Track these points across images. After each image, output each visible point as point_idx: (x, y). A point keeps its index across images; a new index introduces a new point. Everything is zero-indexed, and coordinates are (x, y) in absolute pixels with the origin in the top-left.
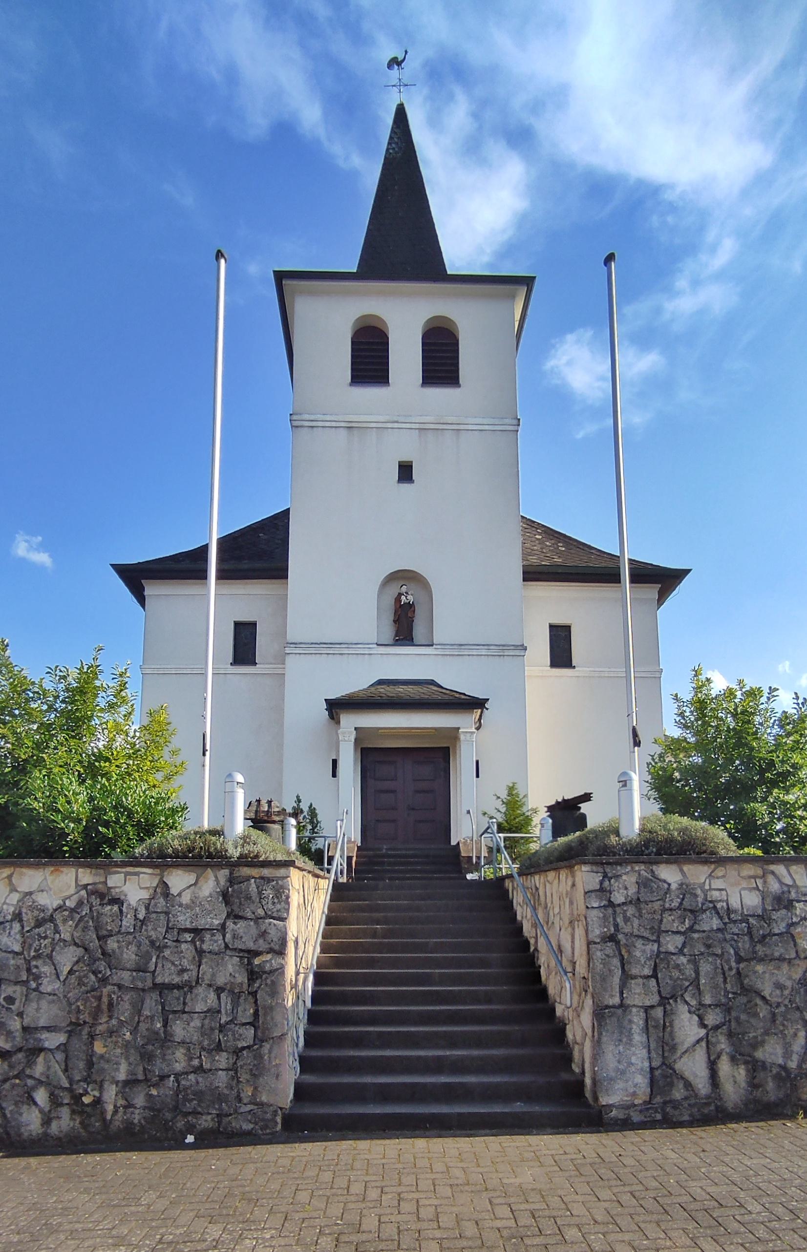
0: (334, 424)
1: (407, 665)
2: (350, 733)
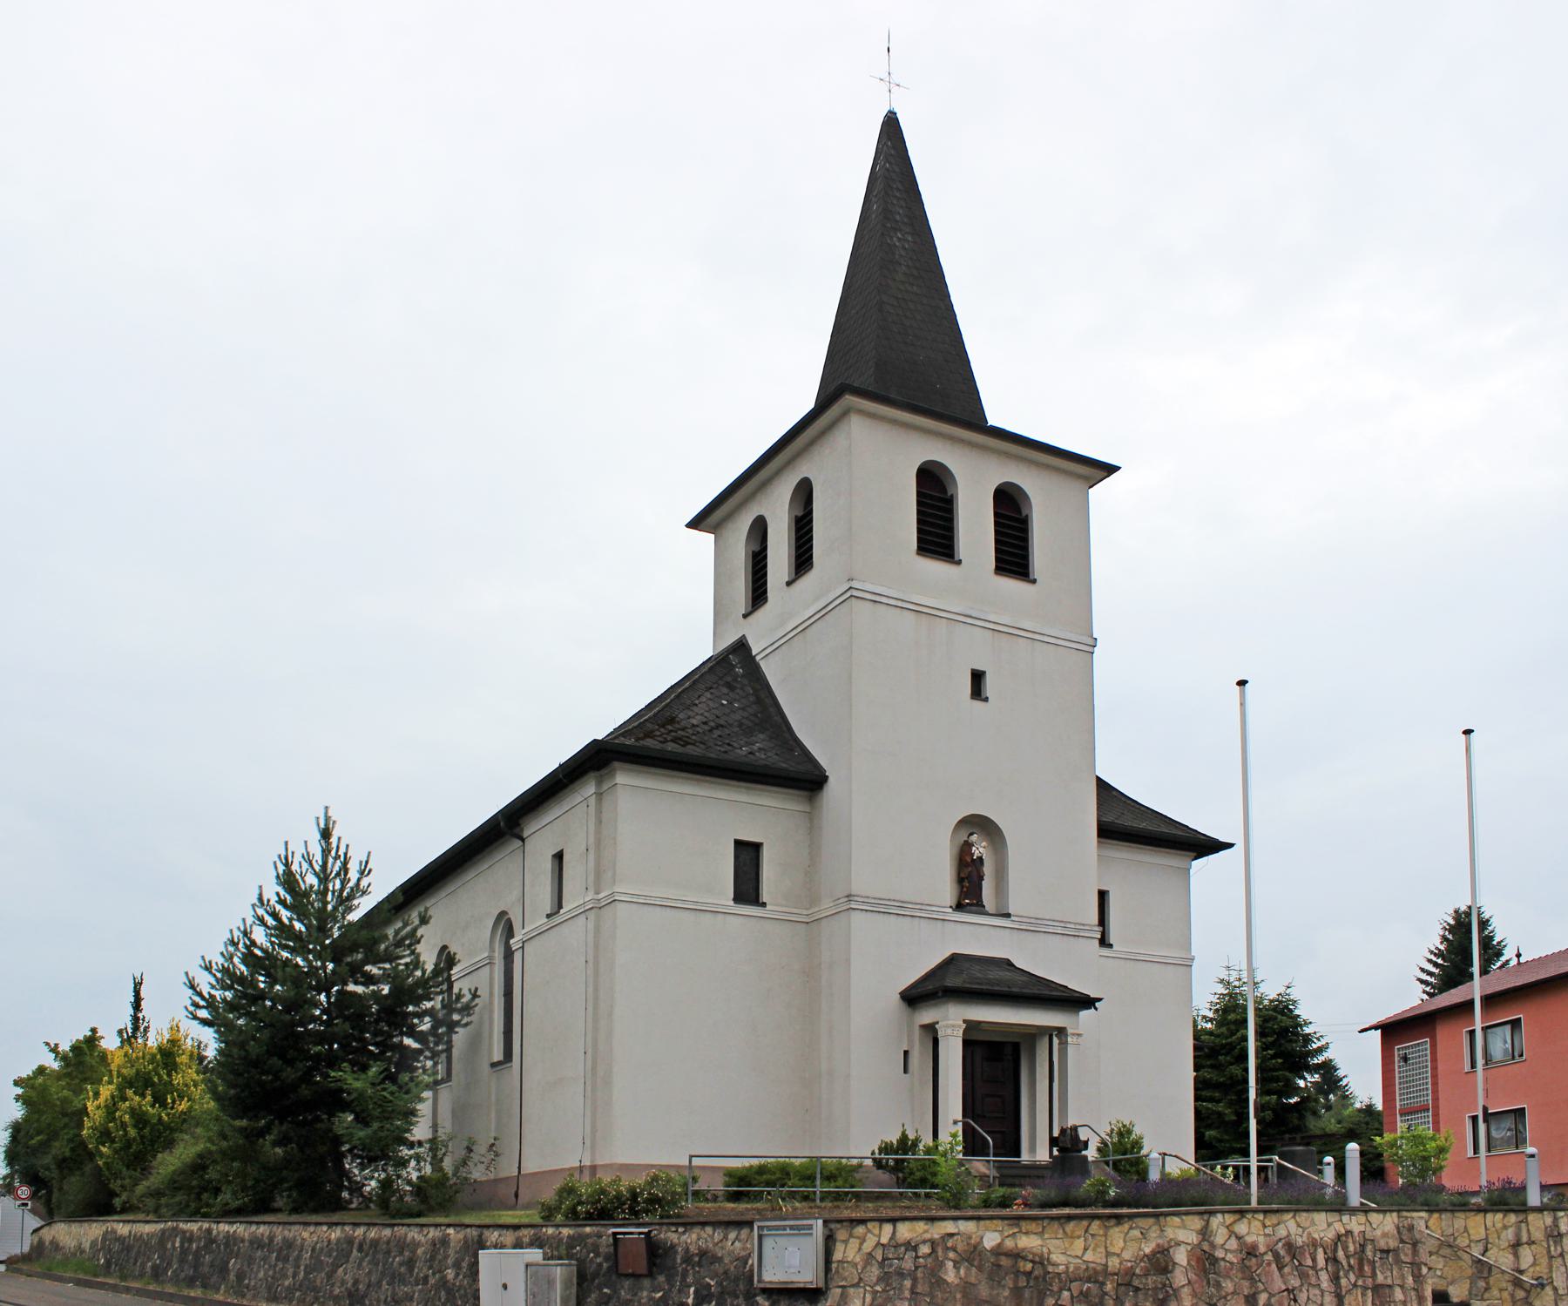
0: (899, 604)
1: (977, 938)
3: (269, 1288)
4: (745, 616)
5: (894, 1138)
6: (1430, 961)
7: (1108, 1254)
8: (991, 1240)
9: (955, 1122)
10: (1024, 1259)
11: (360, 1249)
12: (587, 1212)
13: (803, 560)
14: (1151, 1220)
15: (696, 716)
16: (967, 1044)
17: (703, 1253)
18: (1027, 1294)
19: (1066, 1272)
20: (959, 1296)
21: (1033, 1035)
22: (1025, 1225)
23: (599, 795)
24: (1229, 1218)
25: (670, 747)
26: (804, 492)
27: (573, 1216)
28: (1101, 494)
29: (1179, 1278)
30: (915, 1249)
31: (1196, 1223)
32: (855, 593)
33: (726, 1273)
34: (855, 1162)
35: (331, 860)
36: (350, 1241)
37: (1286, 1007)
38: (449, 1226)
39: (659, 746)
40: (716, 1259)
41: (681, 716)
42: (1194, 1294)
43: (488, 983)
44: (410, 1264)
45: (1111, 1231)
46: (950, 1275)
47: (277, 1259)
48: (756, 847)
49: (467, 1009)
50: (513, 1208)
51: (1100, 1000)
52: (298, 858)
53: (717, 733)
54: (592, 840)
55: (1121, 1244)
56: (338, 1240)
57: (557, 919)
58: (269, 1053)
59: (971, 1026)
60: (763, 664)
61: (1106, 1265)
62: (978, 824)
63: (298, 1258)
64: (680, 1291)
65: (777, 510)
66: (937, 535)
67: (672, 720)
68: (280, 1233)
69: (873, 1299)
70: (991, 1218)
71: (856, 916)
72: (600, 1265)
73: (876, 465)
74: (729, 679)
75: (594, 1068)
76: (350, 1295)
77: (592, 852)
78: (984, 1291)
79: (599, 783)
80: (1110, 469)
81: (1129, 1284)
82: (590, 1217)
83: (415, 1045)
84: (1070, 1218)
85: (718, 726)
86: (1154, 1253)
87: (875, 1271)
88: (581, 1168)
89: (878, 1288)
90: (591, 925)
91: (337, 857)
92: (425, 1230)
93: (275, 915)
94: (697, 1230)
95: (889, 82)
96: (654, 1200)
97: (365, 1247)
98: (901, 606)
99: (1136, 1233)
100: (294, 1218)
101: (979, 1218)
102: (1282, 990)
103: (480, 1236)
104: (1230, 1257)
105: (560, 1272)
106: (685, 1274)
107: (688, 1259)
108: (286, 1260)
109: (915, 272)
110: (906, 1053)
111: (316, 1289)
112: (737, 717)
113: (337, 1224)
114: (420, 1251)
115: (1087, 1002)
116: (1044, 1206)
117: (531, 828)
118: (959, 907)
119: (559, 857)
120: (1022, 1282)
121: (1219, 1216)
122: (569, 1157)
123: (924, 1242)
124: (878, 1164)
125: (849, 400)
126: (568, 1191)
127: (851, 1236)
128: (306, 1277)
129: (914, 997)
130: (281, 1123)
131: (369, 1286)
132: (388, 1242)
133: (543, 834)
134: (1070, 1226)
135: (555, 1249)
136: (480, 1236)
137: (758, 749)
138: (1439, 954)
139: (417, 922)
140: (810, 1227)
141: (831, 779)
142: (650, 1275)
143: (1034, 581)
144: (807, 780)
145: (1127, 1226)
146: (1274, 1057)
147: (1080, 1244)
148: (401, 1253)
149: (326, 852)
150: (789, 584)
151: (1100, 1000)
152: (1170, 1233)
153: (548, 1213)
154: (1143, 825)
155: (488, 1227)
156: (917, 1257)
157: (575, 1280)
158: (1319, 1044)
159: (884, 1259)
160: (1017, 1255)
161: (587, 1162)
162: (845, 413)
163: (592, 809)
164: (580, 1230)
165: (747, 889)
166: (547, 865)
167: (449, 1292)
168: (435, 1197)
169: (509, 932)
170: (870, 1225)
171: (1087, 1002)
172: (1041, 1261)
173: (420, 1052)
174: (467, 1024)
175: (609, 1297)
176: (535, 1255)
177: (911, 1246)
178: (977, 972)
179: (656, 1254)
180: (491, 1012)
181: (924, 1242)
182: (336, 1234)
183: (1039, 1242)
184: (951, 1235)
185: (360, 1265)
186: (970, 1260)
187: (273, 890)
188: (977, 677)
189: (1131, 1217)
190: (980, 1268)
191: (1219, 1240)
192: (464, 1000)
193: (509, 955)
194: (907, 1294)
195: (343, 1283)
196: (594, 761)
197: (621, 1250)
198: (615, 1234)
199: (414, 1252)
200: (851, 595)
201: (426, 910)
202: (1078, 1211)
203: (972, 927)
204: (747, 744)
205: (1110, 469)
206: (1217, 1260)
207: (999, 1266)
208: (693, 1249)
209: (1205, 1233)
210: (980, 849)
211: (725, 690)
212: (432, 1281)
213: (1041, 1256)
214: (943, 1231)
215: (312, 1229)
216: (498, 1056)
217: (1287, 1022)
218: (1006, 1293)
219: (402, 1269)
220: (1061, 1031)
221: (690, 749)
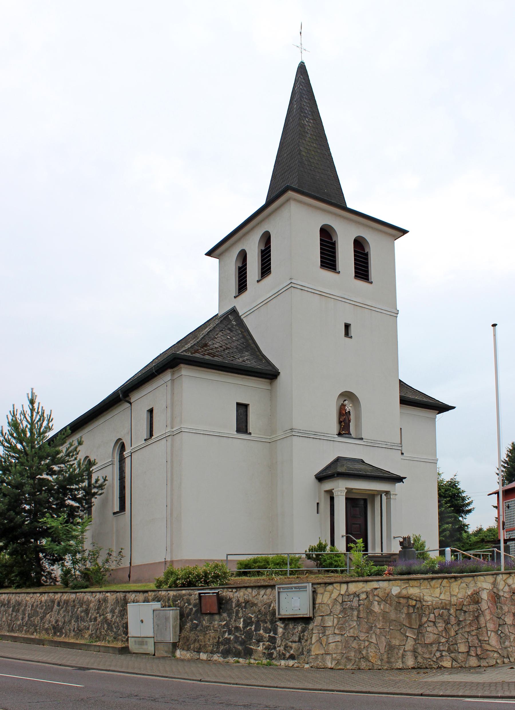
0: (313, 291)
1: (348, 449)
2: (344, 491)
3: (9, 626)
4: (235, 297)
5: (315, 544)
6: (502, 465)
7: (451, 595)
8: (395, 590)
9: (343, 536)
10: (412, 599)
11: (59, 605)
12: (183, 583)
13: (265, 269)
14: (471, 579)
15: (217, 343)
16: (348, 500)
17: (247, 602)
18: (413, 616)
19: (432, 605)
20: (381, 618)
21: (380, 493)
22: (411, 583)
23: (173, 380)
24: (505, 576)
25: (207, 357)
26: (267, 239)
27: (174, 586)
28: (400, 243)
29: (484, 606)
30: (358, 596)
31: (491, 579)
32: (293, 285)
33: (259, 611)
34: (297, 556)
35: (35, 414)
36: (53, 601)
37: (454, 485)
38: (107, 592)
39: (202, 357)
40: (254, 605)
41: (210, 343)
42: (491, 613)
43: (112, 475)
44: (87, 612)
45: (452, 585)
46: (376, 608)
47: (13, 611)
48: (246, 406)
49: (101, 487)
50: (129, 582)
51: (405, 478)
52: (19, 412)
53: (227, 351)
54: (169, 401)
55: (457, 590)
56: (46, 601)
57: (150, 441)
58: (8, 510)
59: (349, 491)
60: (244, 320)
61: (450, 601)
62: (348, 396)
63: (25, 610)
64: (235, 621)
65: (253, 248)
66: (329, 260)
67: (206, 345)
68: (14, 598)
69: (338, 622)
70: (395, 580)
71: (294, 438)
72: (191, 609)
73: (299, 226)
74: (229, 326)
75: (171, 514)
76: (54, 628)
77: (169, 409)
78: (393, 616)
79: (173, 374)
80: (404, 232)
81: (461, 610)
82: (183, 585)
83: (77, 505)
84: (433, 579)
85: (227, 348)
86: (472, 594)
87: (338, 608)
88: (165, 562)
89: (340, 616)
90: (169, 443)
91: (38, 413)
92: (94, 594)
93: (8, 441)
94: (243, 590)
95: (301, 48)
96: (217, 577)
97: (61, 604)
98: (313, 292)
99: (464, 585)
100: (18, 590)
101: (389, 580)
102: (452, 477)
103: (125, 596)
104: (505, 595)
105: (172, 614)
106: (237, 613)
107: (238, 605)
108: (18, 611)
109: (314, 138)
110: (318, 504)
111: (35, 626)
112: (235, 344)
113: (45, 593)
114: (91, 605)
115: (400, 479)
116: (401, 574)
117: (134, 397)
118: (339, 434)
119: (151, 411)
120: (411, 610)
121: (500, 575)
122: (160, 556)
123: (363, 593)
124: (309, 557)
125: (290, 193)
126: (171, 573)
127: (325, 591)
128: (29, 619)
129: (321, 478)
130: (13, 544)
131: (64, 623)
132: (74, 601)
133: (142, 400)
134: (433, 582)
135: (168, 603)
136: (125, 596)
137: (245, 359)
138: (506, 462)
139: (77, 444)
140: (305, 587)
141: (281, 373)
142: (219, 613)
143: (371, 283)
144: (270, 374)
145: (459, 582)
146: (450, 507)
147: (438, 591)
148: (81, 606)
149: (32, 410)
150: (258, 281)
151: (405, 478)
152: (479, 584)
153: (160, 584)
154: (416, 398)
155: (129, 592)
156: (359, 600)
157: (179, 617)
158: (468, 501)
159: (343, 602)
160: (408, 598)
161: (168, 559)
162: (288, 200)
163: (169, 387)
164: (180, 592)
165: (242, 427)
166: (145, 416)
167: (109, 624)
168: (91, 579)
169: (123, 447)
170: (335, 585)
171: (400, 479)
172: (420, 600)
173: (78, 507)
174: (101, 494)
175: (197, 625)
176: (157, 605)
177: (356, 595)
178: (350, 465)
179: (222, 604)
180: (113, 487)
181: (363, 593)
182: (45, 598)
183: (418, 591)
184: (376, 589)
185: (59, 612)
186: (385, 601)
187: (6, 429)
188: (347, 327)
189: (461, 577)
190: (390, 605)
191: (501, 587)
192: (100, 482)
193: (122, 460)
194: (355, 618)
195: (50, 622)
196: (169, 363)
197: (203, 601)
198: (200, 594)
199: (88, 606)
200: (291, 286)
201: (81, 437)
202: (447, 575)
203: (222, 438)
204: (241, 357)
205: (404, 232)
206: (500, 596)
207: (400, 603)
208: (241, 600)
209: (494, 584)
210: (349, 407)
211: (229, 332)
212: (99, 620)
213: (420, 598)
214: (372, 587)
215: (31, 595)
216: (117, 509)
217: (455, 491)
218: (404, 616)
219: (83, 614)
220: (387, 493)
221: (216, 359)
